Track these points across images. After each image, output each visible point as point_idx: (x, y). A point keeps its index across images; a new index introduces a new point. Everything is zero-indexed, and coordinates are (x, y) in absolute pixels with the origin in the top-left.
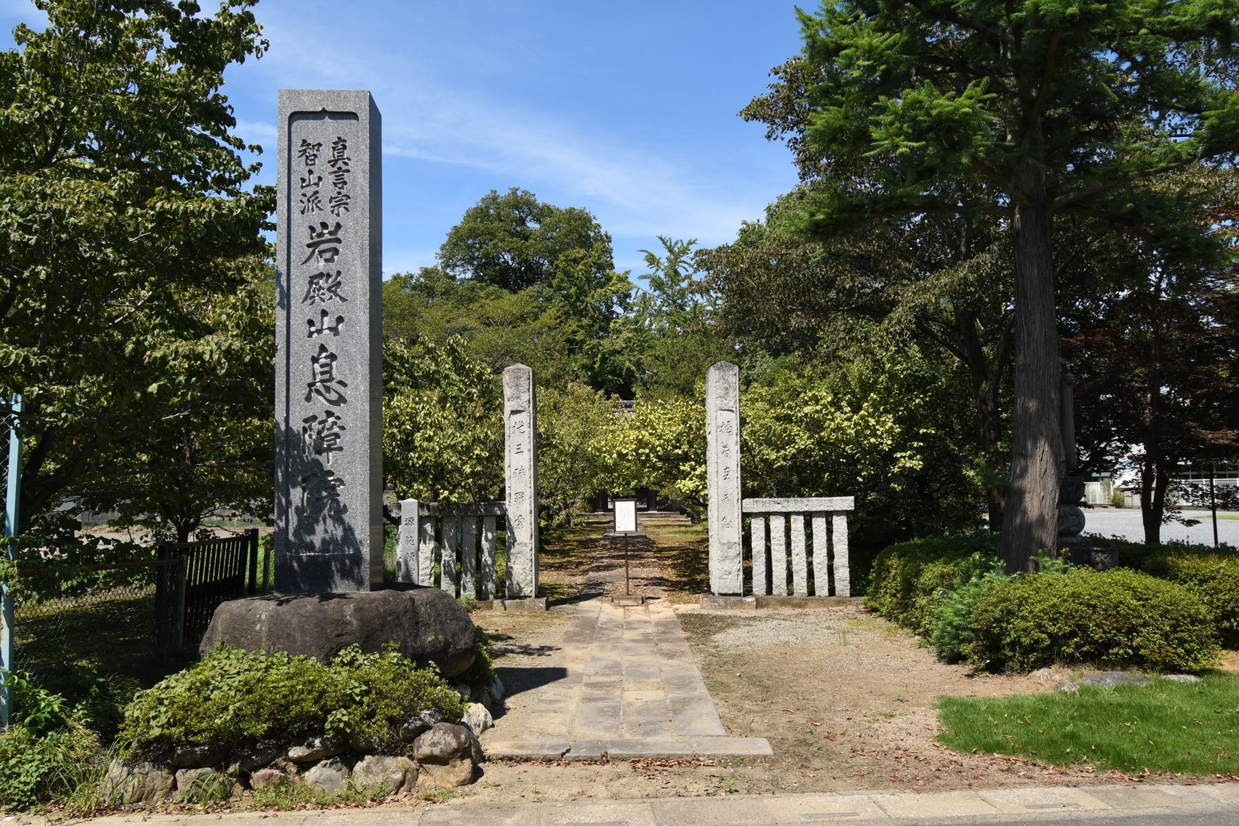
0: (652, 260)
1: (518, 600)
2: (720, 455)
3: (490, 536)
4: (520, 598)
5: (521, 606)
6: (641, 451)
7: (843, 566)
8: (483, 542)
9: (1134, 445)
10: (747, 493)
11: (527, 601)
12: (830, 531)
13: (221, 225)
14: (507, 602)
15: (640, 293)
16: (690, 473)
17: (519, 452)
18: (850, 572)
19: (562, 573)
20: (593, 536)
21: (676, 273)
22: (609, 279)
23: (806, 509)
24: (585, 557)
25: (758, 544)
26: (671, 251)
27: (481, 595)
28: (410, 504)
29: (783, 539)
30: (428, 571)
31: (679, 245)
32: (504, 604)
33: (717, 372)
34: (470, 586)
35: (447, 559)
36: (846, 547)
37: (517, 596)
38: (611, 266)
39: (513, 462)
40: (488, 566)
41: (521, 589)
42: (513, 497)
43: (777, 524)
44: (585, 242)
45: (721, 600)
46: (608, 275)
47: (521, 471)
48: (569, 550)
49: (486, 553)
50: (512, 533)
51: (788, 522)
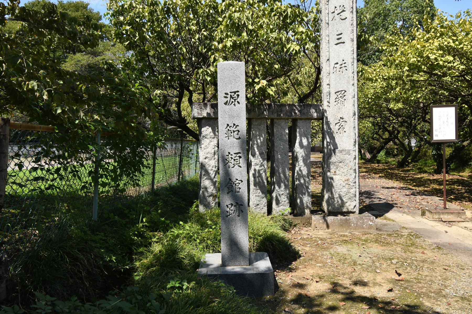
1: (340, 217)
4: (343, 214)
14: (330, 219)
17: (340, 42)
34: (284, 199)
35: (257, 168)
39: (332, 55)
40: (303, 176)
41: (343, 203)
50: (332, 138)
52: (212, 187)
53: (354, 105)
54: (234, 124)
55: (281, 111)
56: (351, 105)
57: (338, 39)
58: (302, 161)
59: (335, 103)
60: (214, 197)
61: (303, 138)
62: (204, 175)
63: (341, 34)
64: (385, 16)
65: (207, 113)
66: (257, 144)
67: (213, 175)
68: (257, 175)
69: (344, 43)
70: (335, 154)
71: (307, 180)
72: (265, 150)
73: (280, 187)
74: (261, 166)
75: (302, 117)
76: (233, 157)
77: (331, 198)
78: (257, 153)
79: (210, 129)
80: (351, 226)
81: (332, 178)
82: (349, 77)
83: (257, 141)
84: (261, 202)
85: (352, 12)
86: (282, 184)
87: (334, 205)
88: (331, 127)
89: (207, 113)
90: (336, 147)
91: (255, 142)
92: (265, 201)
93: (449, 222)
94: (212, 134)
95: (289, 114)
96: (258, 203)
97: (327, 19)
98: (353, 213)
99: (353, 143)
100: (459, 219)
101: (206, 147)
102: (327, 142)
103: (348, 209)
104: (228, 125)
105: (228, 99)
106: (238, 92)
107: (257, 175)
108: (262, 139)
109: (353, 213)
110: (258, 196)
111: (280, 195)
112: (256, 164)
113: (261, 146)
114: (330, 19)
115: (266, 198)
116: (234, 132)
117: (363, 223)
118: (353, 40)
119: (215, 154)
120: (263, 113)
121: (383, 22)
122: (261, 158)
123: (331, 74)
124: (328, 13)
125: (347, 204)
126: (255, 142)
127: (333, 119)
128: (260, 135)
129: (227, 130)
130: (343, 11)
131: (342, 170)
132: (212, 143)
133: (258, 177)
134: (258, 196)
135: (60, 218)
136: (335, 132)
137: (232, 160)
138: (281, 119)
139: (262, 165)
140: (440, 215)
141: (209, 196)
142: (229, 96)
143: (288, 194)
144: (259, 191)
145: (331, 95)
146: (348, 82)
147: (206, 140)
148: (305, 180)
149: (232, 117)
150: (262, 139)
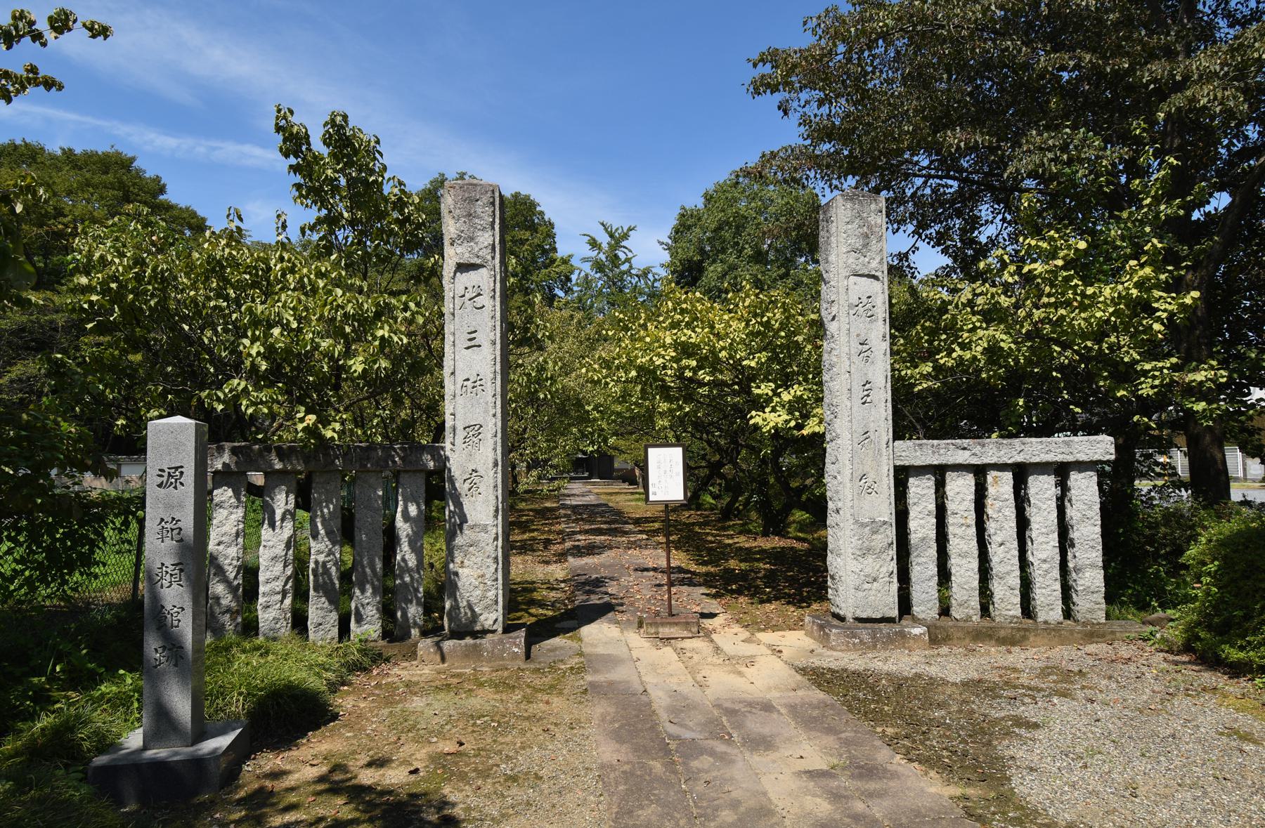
0: (594, 244)
1: (469, 641)
2: (855, 358)
3: (413, 510)
4: (476, 635)
5: (475, 653)
6: (684, 362)
7: (1092, 566)
8: (400, 522)
9: (1258, 389)
10: (900, 432)
11: (486, 642)
12: (1021, 501)
13: (245, 273)
14: (448, 645)
15: (583, 274)
16: (769, 400)
17: (473, 345)
18: (1106, 577)
19: (529, 558)
20: (548, 505)
21: (616, 256)
22: (553, 261)
23: (1019, 458)
24: (550, 532)
25: (922, 526)
26: (611, 236)
27: (394, 632)
28: (172, 429)
29: (971, 518)
30: (278, 585)
31: (620, 231)
32: (440, 649)
33: (849, 205)
34: (371, 612)
35: (321, 558)
36: (1098, 529)
37: (467, 629)
38: (555, 250)
39: (460, 365)
40: (409, 570)
41: (475, 617)
42: (461, 434)
43: (960, 488)
44: (533, 228)
45: (865, 633)
46: (552, 257)
47: (476, 383)
48: (527, 521)
49: (405, 547)
50: (459, 505)
51: (1063, 485)
52: (230, 597)
53: (495, 449)
54: (173, 519)
55: (368, 459)
56: (490, 449)
57: (470, 340)
58: (406, 544)
59: (464, 446)
60: (232, 613)
61: (410, 504)
62: (215, 575)
63: (476, 331)
64: (737, 227)
65: (224, 463)
66: (323, 515)
67: (234, 574)
68: (320, 570)
69: (480, 346)
70: (461, 532)
71: (416, 576)
72: (336, 525)
73: (363, 591)
74: (328, 555)
75: (408, 468)
76: (168, 570)
77: (456, 607)
78: (322, 532)
79: (230, 492)
80: (483, 655)
81: (456, 574)
82: (487, 403)
83: (322, 511)
84: (328, 619)
85: (493, 297)
86: (368, 586)
87: (460, 620)
88: (457, 485)
89: (224, 463)
90: (464, 519)
91: (319, 513)
92: (334, 617)
93: (668, 639)
94: (233, 500)
95: (382, 463)
96: (320, 620)
97: (452, 306)
98: (494, 632)
99: (492, 513)
100: (685, 634)
101: (222, 524)
102: (450, 511)
103: (483, 625)
104: (162, 520)
105: (165, 479)
106: (182, 467)
107: (320, 570)
108: (331, 506)
109: (494, 632)
110: (322, 609)
111: (363, 605)
112: (319, 552)
113: (330, 519)
114: (457, 307)
115: (337, 611)
116: (172, 530)
117: (503, 651)
118: (494, 343)
119: (237, 535)
120: (333, 462)
121: (734, 238)
122: (330, 540)
123: (457, 398)
124: (454, 298)
125: (482, 618)
126: (319, 513)
127: (460, 472)
128: (328, 501)
129: (160, 527)
130: (479, 295)
131: (473, 558)
132: (233, 517)
133: (322, 574)
134: (322, 609)
135: (989, 377)
136: (463, 494)
137: (168, 575)
138: (368, 471)
139: (330, 553)
140: (657, 627)
141: (223, 613)
142: (166, 474)
143: (379, 603)
144: (323, 599)
145: (457, 432)
146: (486, 411)
147: (221, 510)
148: (412, 578)
149: (169, 506)
150: (331, 506)
